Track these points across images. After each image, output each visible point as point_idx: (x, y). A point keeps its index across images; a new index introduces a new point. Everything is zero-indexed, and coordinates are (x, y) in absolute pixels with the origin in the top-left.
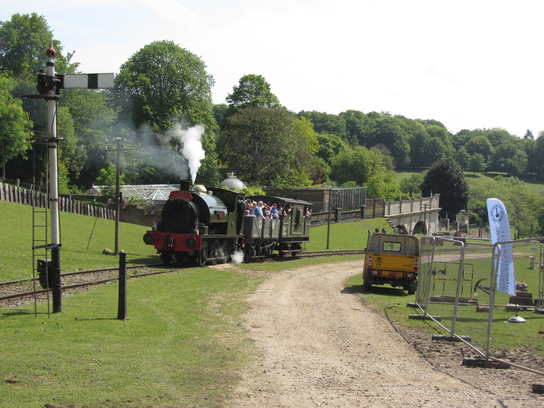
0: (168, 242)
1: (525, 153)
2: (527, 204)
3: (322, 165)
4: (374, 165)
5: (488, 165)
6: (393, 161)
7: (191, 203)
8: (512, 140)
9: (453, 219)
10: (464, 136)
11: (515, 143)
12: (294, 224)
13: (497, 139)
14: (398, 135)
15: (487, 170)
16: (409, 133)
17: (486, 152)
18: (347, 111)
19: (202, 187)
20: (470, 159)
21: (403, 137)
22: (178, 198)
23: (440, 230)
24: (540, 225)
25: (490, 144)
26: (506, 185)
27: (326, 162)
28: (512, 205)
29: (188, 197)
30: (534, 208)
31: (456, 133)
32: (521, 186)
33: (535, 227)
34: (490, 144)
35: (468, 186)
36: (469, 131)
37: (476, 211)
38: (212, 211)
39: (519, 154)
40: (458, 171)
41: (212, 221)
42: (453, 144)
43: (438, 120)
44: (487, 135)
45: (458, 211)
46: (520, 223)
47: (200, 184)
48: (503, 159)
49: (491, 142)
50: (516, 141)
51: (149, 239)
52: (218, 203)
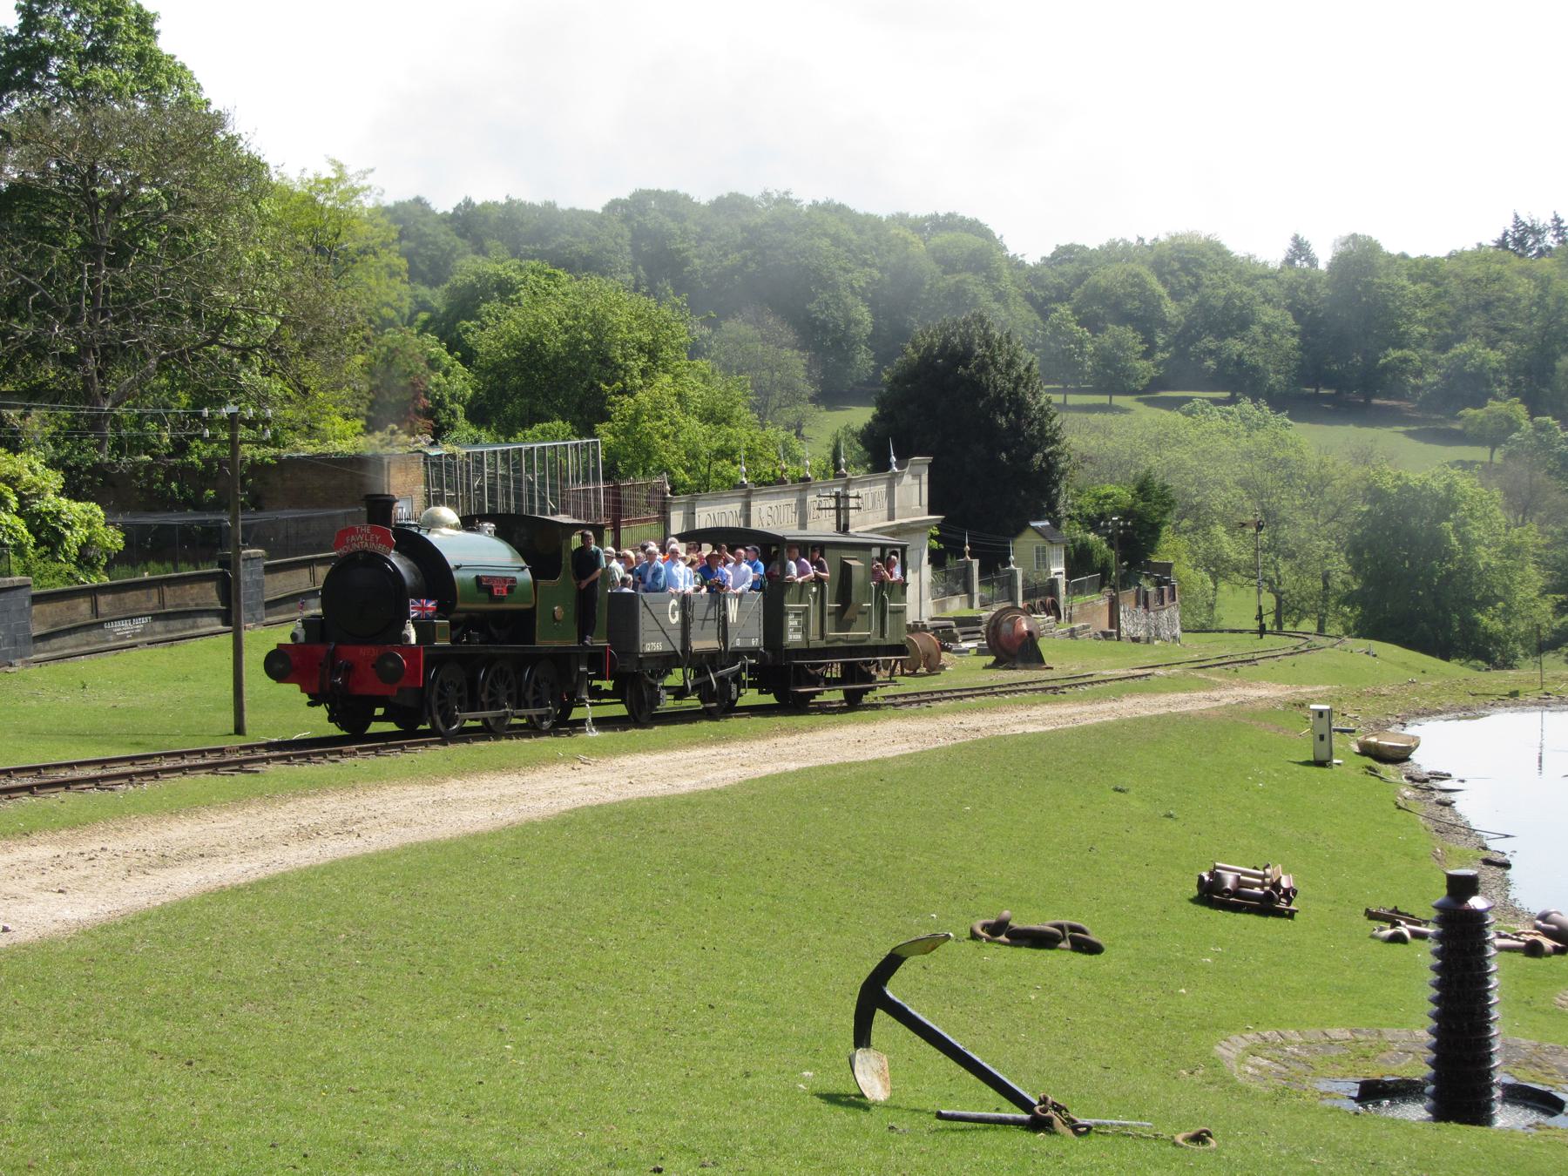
1: (1289, 316)
2: (1304, 496)
3: (433, 364)
4: (652, 352)
5: (1157, 366)
6: (808, 368)
7: (394, 558)
8: (1239, 272)
9: (994, 561)
10: (1068, 268)
11: (1250, 284)
12: (831, 605)
13: (1189, 272)
14: (825, 274)
15: (1156, 384)
16: (865, 263)
17: (1146, 321)
18: (633, 196)
20: (1090, 348)
21: (841, 278)
23: (941, 606)
25: (1161, 290)
27: (450, 351)
28: (1248, 504)
31: (1038, 260)
32: (1283, 432)
33: (1336, 583)
34: (1161, 290)
35: (1057, 421)
36: (1083, 248)
37: (1093, 523)
39: (1266, 319)
42: (1030, 298)
43: (969, 215)
44: (1151, 258)
45: (1020, 528)
46: (1284, 567)
48: (1209, 342)
49: (1165, 283)
50: (1257, 277)
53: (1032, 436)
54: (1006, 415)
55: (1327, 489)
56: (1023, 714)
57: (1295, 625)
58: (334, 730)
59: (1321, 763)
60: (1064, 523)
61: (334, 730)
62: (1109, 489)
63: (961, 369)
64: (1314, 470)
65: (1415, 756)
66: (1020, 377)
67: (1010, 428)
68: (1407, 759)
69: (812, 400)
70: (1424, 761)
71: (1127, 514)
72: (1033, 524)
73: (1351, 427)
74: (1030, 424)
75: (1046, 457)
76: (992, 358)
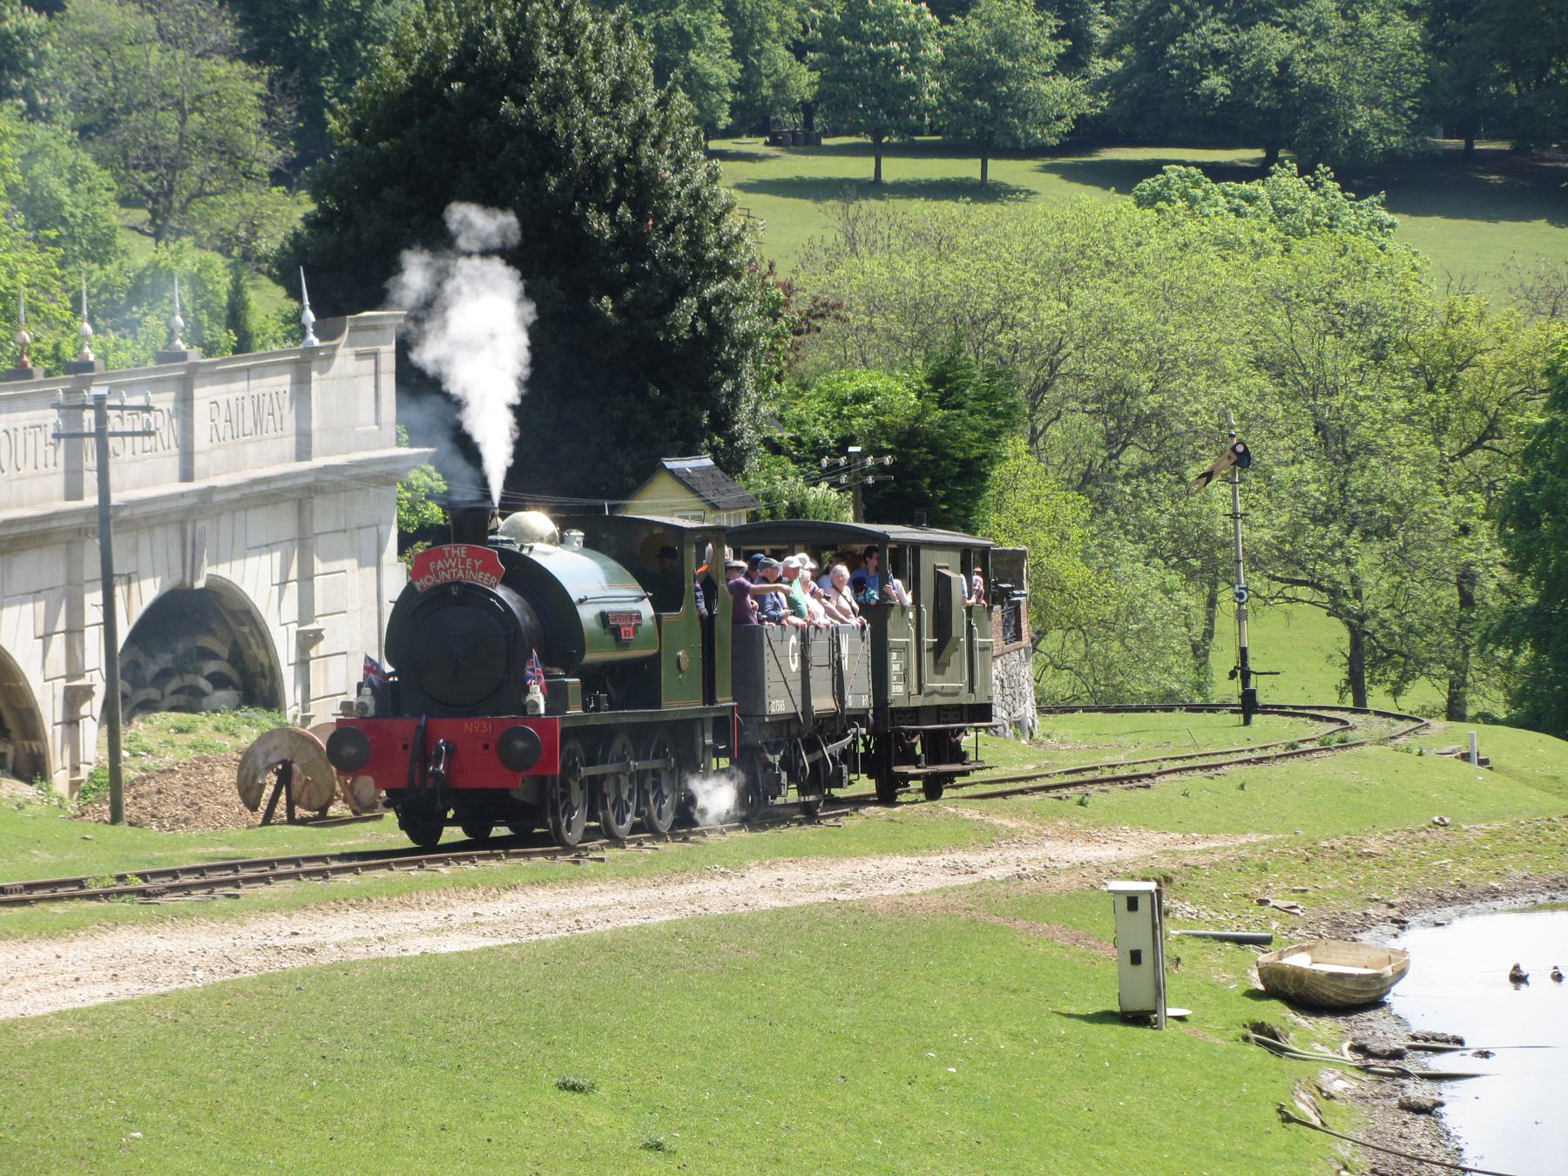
0: (425, 752)
5: (1096, 88)
7: (501, 592)
12: (928, 640)
15: (1088, 134)
19: (538, 521)
20: (934, 50)
22: (445, 576)
24: (1518, 566)
26: (1226, 245)
29: (488, 567)
30: (1476, 423)
32: (1363, 244)
35: (733, 223)
38: (587, 614)
40: (621, 93)
41: (591, 657)
46: (1368, 558)
47: (521, 508)
51: (350, 751)
52: (612, 580)
53: (675, 260)
54: (611, 209)
55: (1467, 374)
56: (427, 918)
57: (1396, 692)
58: (411, 845)
59: (1139, 1018)
60: (753, 463)
61: (411, 845)
62: (864, 380)
63: (507, 106)
64: (1434, 331)
65: (1398, 998)
66: (643, 123)
67: (617, 242)
68: (1376, 1003)
69: (277, 177)
70: (1415, 1005)
71: (908, 438)
72: (672, 464)
73: (1542, 224)
74: (669, 229)
75: (704, 306)
76: (581, 79)
